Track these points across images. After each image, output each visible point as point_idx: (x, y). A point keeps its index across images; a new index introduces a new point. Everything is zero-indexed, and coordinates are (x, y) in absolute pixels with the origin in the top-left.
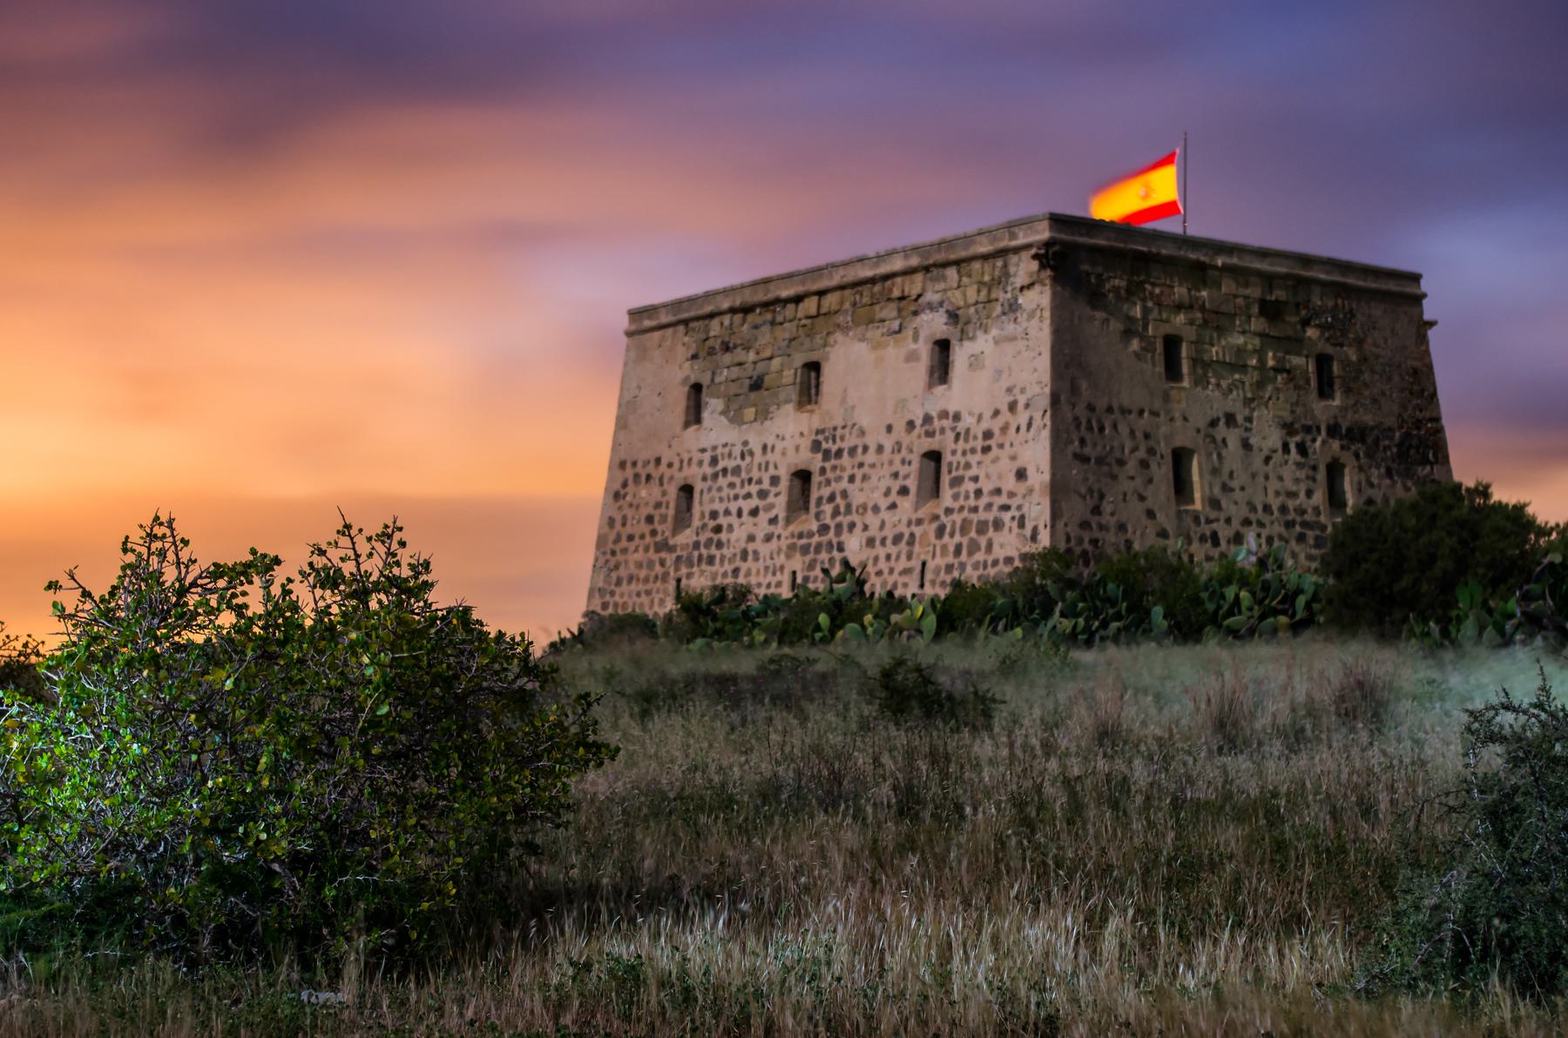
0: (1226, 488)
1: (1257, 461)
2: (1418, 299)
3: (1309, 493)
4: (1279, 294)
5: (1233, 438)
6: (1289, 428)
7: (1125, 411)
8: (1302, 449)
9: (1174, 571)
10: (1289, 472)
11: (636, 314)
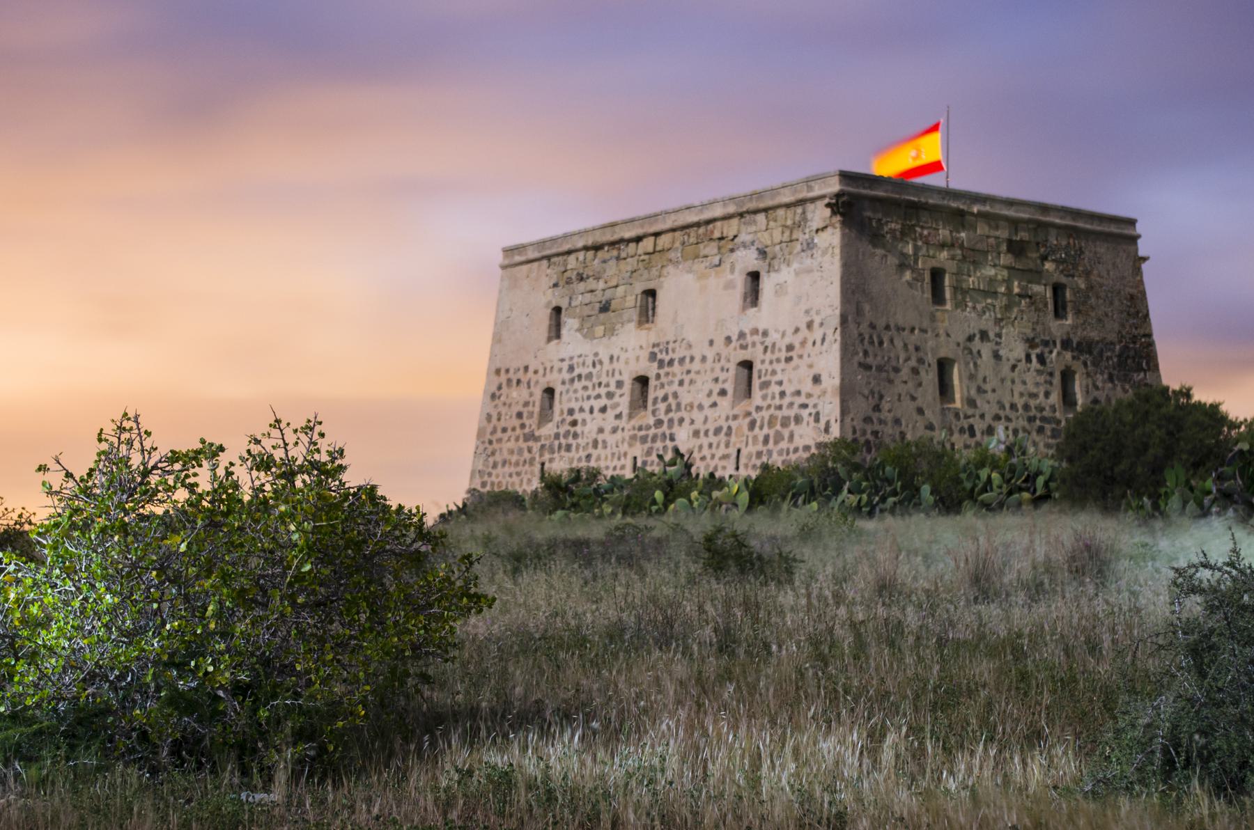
0: (980, 390)
1: (1006, 369)
2: (1134, 239)
3: (1047, 395)
4: (1023, 235)
5: (986, 350)
6: (1031, 343)
7: (900, 329)
8: (1041, 359)
9: (940, 457)
10: (1031, 377)
11: (508, 251)
